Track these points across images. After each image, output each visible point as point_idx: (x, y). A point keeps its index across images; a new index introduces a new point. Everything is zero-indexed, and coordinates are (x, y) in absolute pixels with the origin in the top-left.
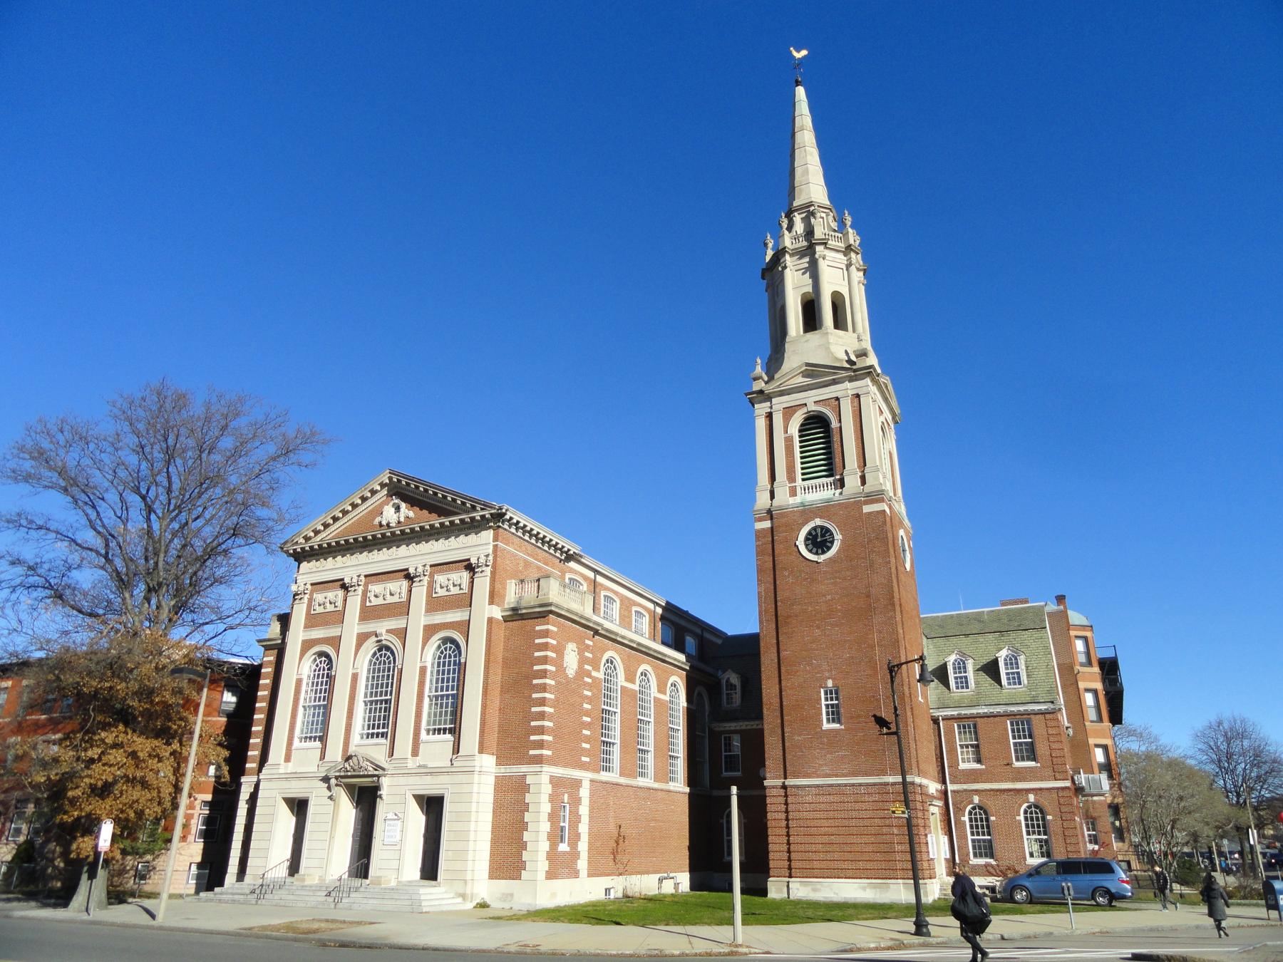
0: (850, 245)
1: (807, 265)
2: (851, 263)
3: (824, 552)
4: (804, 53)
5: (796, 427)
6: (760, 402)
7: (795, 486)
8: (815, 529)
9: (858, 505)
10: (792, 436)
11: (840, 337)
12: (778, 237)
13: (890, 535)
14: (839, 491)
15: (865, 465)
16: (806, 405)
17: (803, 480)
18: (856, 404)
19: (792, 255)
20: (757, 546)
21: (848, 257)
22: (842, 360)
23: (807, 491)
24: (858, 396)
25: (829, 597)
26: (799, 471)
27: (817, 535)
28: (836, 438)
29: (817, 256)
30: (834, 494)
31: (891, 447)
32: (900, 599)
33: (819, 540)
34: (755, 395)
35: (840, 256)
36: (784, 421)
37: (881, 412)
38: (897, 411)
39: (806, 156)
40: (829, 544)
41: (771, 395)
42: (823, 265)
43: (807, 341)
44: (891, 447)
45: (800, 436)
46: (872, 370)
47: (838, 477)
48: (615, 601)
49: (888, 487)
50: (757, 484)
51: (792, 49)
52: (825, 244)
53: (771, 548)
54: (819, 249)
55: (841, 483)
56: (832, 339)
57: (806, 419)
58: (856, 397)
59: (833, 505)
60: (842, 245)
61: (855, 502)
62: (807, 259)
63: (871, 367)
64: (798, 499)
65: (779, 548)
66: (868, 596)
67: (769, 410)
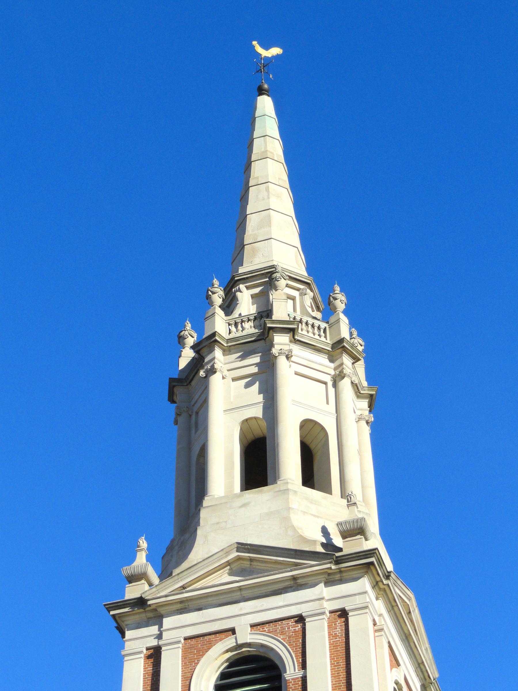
0: (342, 340)
1: (255, 370)
2: (341, 372)
4: (276, 51)
6: (138, 626)
16: (233, 631)
18: (339, 630)
19: (227, 351)
21: (338, 363)
24: (343, 614)
29: (275, 351)
35: (323, 360)
36: (185, 665)
37: (396, 662)
38: (433, 672)
39: (269, 198)
41: (162, 610)
43: (244, 505)
46: (373, 559)
51: (255, 43)
52: (293, 331)
57: (233, 663)
58: (340, 616)
62: (256, 359)
63: (373, 552)
67: (154, 643)
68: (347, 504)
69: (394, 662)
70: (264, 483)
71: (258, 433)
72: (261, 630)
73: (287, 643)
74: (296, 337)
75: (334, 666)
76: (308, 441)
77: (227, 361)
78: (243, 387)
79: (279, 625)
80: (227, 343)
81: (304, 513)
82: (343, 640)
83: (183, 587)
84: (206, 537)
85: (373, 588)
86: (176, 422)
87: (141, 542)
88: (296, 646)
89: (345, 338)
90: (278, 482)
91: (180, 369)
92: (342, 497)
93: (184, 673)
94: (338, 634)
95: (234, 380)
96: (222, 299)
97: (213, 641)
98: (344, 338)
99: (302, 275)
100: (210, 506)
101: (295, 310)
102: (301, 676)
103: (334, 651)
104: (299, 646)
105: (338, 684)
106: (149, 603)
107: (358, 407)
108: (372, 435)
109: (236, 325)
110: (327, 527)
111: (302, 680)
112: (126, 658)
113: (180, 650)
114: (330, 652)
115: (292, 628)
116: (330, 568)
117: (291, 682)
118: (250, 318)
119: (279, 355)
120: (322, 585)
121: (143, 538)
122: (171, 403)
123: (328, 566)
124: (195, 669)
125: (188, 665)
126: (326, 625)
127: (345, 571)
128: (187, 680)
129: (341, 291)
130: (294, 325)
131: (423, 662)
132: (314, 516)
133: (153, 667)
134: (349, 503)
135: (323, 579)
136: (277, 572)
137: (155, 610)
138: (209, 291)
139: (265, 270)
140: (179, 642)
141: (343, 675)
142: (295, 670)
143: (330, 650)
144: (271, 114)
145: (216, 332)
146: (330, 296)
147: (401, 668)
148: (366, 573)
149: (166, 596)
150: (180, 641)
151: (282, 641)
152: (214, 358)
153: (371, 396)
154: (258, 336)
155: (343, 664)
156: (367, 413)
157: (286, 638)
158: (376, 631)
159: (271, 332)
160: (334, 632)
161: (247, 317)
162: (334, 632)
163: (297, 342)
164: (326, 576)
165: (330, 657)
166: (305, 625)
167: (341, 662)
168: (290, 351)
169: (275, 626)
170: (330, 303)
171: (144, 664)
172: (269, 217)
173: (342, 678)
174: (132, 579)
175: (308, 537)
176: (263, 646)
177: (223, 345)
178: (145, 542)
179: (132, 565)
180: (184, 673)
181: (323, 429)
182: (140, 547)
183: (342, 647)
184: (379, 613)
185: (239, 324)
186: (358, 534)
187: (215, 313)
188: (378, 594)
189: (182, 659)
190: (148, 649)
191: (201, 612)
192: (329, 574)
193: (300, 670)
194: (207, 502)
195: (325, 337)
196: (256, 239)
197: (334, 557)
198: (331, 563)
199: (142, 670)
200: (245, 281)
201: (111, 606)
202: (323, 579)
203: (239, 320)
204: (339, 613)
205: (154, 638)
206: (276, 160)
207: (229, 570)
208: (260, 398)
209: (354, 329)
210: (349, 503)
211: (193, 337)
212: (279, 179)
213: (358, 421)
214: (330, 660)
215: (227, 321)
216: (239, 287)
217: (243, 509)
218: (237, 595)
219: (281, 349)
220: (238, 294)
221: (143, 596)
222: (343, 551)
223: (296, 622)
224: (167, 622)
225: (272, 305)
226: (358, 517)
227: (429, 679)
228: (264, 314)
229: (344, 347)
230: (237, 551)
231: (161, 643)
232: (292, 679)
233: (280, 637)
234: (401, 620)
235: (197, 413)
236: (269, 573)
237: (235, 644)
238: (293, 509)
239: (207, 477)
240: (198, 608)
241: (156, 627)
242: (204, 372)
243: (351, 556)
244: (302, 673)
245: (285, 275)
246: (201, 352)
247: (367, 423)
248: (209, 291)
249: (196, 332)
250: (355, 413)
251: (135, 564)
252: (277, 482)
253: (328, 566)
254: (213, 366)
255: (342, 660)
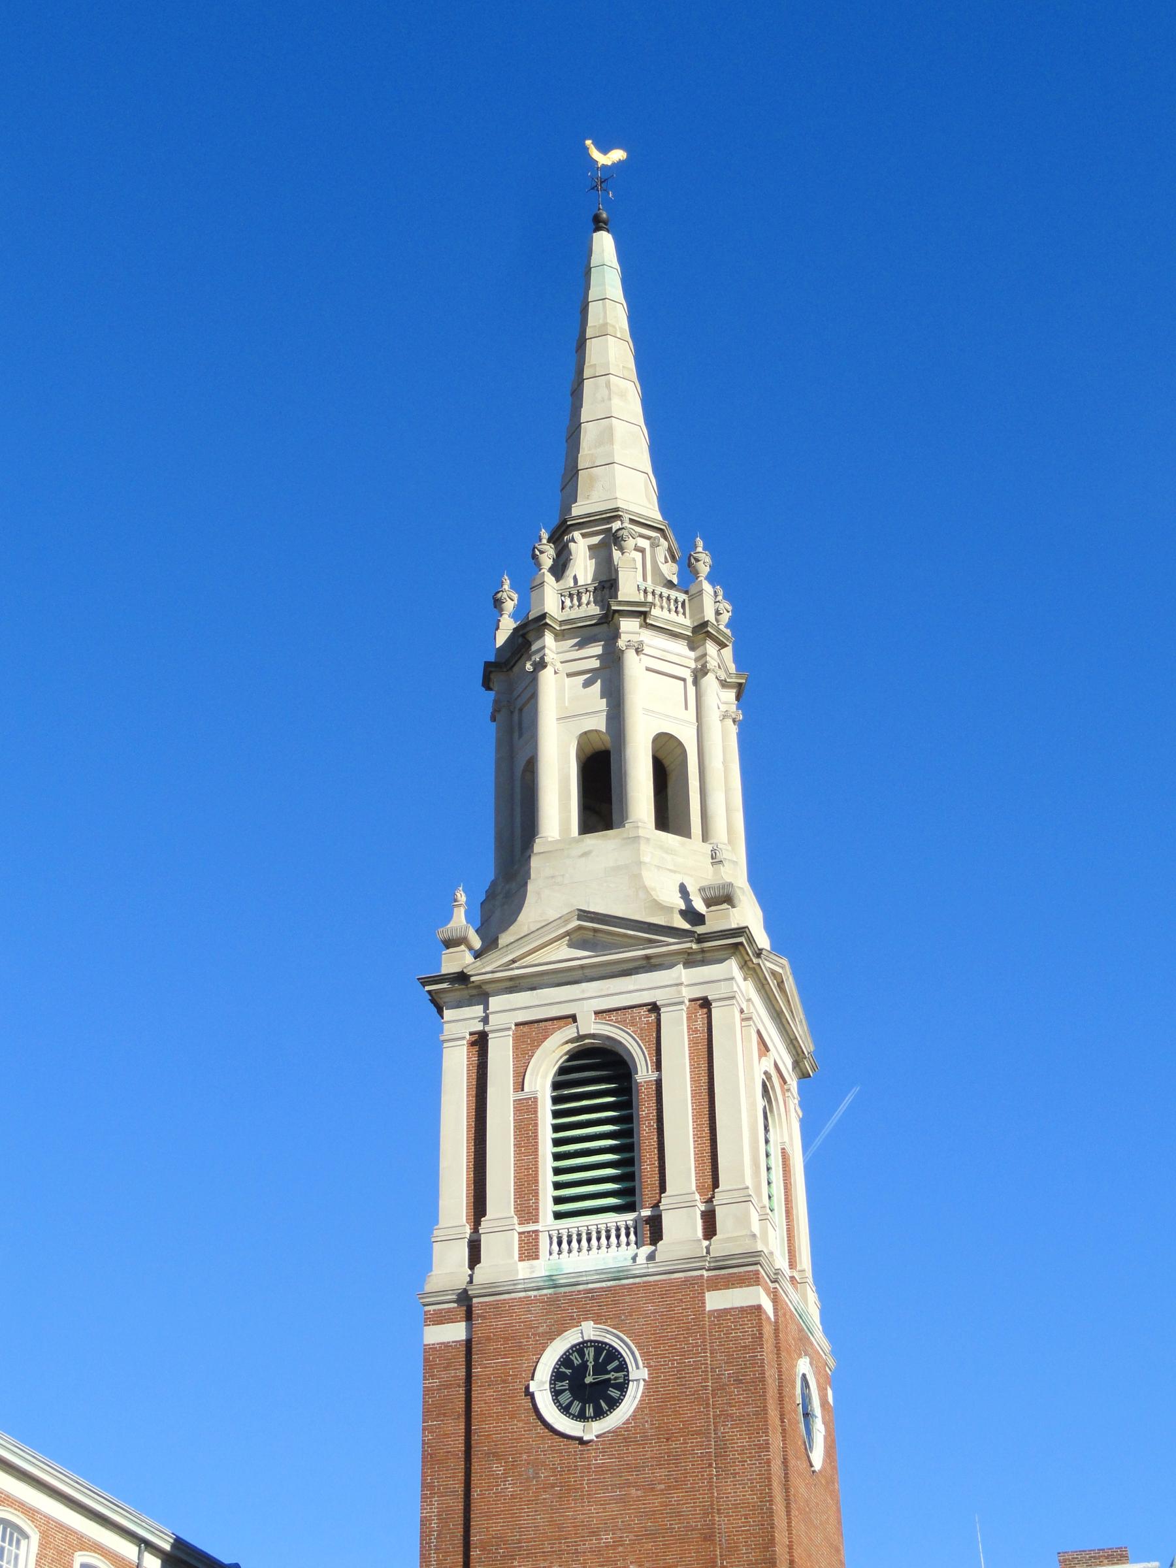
0: (705, 624)
1: (596, 664)
2: (704, 666)
3: (599, 1414)
4: (618, 155)
5: (545, 1077)
6: (459, 1005)
7: (536, 1231)
8: (579, 1348)
9: (695, 1289)
10: (536, 1098)
11: (668, 851)
12: (529, 587)
13: (771, 1373)
14: (646, 1250)
15: (716, 1184)
16: (574, 1018)
17: (558, 1216)
18: (700, 1024)
19: (560, 636)
20: (427, 1391)
21: (699, 652)
22: (668, 910)
23: (565, 1245)
24: (705, 1003)
25: (607, 1538)
26: (547, 1193)
27: (584, 1365)
28: (645, 1110)
29: (621, 643)
30: (634, 1258)
31: (786, 1139)
32: (790, 1547)
33: (589, 1380)
34: (445, 985)
35: (681, 647)
36: (516, 1058)
37: (764, 1048)
38: (807, 1045)
39: (610, 399)
40: (614, 1393)
41: (487, 988)
42: (634, 665)
43: (585, 854)
44: (786, 1139)
45: (556, 1100)
46: (742, 939)
47: (646, 1213)
48: (27, 1537)
49: (774, 1246)
50: (437, 1223)
51: (588, 142)
52: (644, 615)
53: (462, 1397)
54: (628, 626)
55: (654, 1230)
56: (648, 854)
57: (573, 1056)
58: (702, 1006)
59: (630, 1288)
60: (684, 622)
61: (686, 1280)
62: (597, 649)
63: (742, 931)
64: (541, 1268)
65: (482, 1397)
66: (709, 1537)
67: (479, 1027)
68: (711, 861)
69: (763, 1048)
70: (608, 826)
71: (599, 746)
72: (608, 1019)
73: (638, 1037)
74: (648, 621)
75: (694, 1068)
76: (661, 756)
77: (559, 651)
78: (716, 1236)
79: (628, 1015)
80: (560, 626)
81: (659, 867)
82: (705, 1036)
83: (514, 961)
84: (539, 894)
85: (740, 968)
86: (493, 719)
87: (459, 895)
88: (648, 1042)
89: (748, 929)
90: (626, 825)
91: (497, 647)
92: (703, 841)
93: (516, 1067)
94: (756, 1311)
95: (569, 675)
96: (552, 560)
97: (549, 1029)
98: (708, 621)
99: (653, 520)
100: (542, 853)
101: (645, 579)
102: (655, 1078)
103: (694, 1050)
104: (653, 1041)
105: (699, 1090)
106: (472, 979)
107: (723, 699)
108: (739, 735)
109: (571, 596)
110: (685, 884)
111: (656, 1084)
112: (445, 1045)
113: (511, 1039)
114: (690, 1050)
115: (644, 1018)
116: (691, 948)
117: (643, 1086)
118: (588, 589)
119: (626, 649)
120: (681, 966)
121: (461, 888)
122: (486, 690)
123: (688, 945)
124: (529, 1063)
125: (520, 1057)
126: (685, 1016)
127: (708, 951)
128: (520, 1076)
129: (704, 549)
130: (646, 607)
131: (796, 1038)
132: (671, 871)
133: (478, 1057)
134: (714, 861)
135: (682, 960)
136: (626, 949)
137: (479, 987)
138: (536, 550)
139: (606, 513)
140: (509, 1029)
141: (705, 1079)
142: (648, 1072)
143: (689, 1047)
144: (612, 261)
145: (546, 613)
146: (691, 555)
147: (772, 1056)
148: (733, 954)
149: (493, 972)
150: (510, 1028)
151: (632, 1034)
152: (544, 647)
153: (740, 685)
154: (599, 619)
155: (704, 1066)
156: (734, 708)
157: (637, 1031)
158: (743, 1020)
159: (616, 615)
160: (695, 1025)
161: (584, 587)
162: (695, 1025)
163: (649, 626)
164: (686, 956)
165: (690, 1056)
166: (660, 1015)
167: (702, 1064)
168: (641, 643)
169: (624, 1015)
170: (690, 565)
171: (467, 1052)
172: (610, 429)
173: (703, 1083)
174: (449, 943)
175: (664, 901)
176: (609, 1038)
177: (555, 629)
178: (463, 895)
179: (449, 926)
180: (516, 1067)
181: (680, 744)
182: (458, 902)
183: (704, 1045)
184: (747, 998)
185: (575, 596)
186: (724, 902)
187: (544, 582)
188: (747, 974)
189: (513, 1049)
190: (471, 1034)
191: (535, 991)
192: (689, 954)
193: (653, 1072)
194: (538, 847)
195: (684, 614)
196: (594, 462)
197: (696, 935)
198: (691, 941)
199: (466, 1060)
200: (581, 526)
201: (426, 980)
202: (682, 960)
203: (574, 592)
204: (701, 1001)
205: (479, 1021)
206: (619, 337)
207: (568, 941)
208: (602, 704)
209: (718, 587)
210: (714, 861)
211: (513, 600)
212: (623, 367)
213: (723, 719)
214: (690, 1059)
215: (560, 592)
216: (573, 535)
217: (583, 859)
218: (578, 974)
219: (629, 641)
220: (572, 545)
221: (465, 971)
222: (705, 924)
223: (649, 1011)
224: (495, 1002)
225: (617, 571)
226: (724, 880)
227: (802, 1054)
228: (607, 585)
229: (708, 631)
230: (578, 920)
231: (487, 1029)
232: (645, 1082)
233: (630, 1029)
234: (773, 999)
235: (521, 710)
236: (617, 951)
237: (576, 1035)
238: (645, 863)
239: (538, 811)
240: (530, 987)
241: (481, 1007)
242: (531, 665)
243: (716, 934)
244: (657, 1075)
245: (634, 533)
246: (527, 636)
247: (734, 721)
248: (536, 550)
249: (517, 592)
250: (719, 708)
251: (452, 924)
252: (624, 825)
253: (688, 945)
254: (542, 658)
255: (704, 1061)
